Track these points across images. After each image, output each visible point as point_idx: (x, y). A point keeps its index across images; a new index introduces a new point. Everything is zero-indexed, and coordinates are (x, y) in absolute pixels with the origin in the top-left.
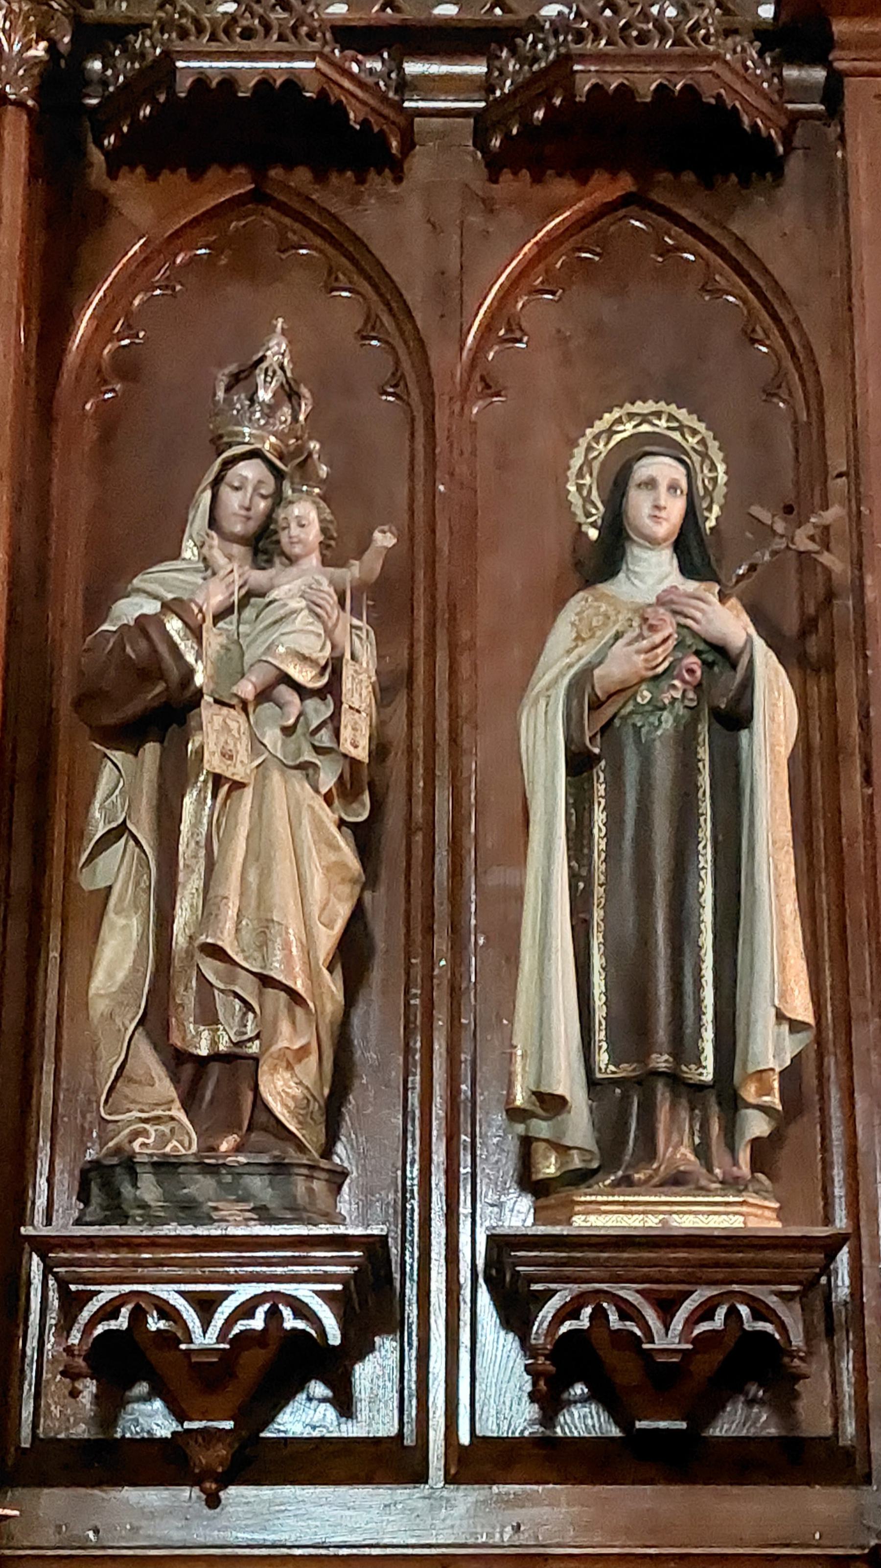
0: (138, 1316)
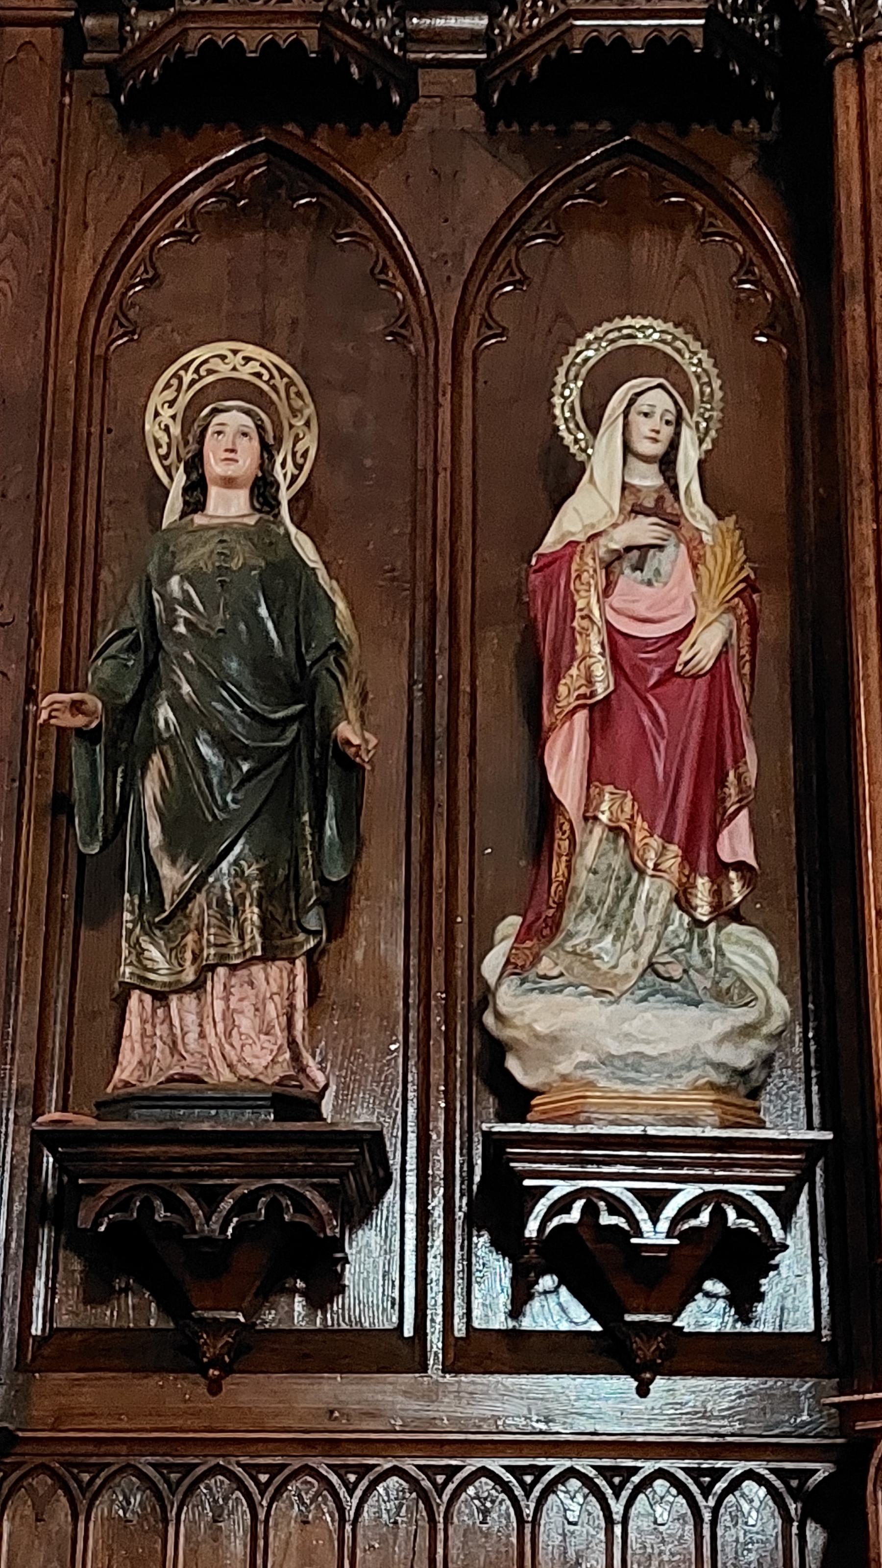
0: (590, 1211)
